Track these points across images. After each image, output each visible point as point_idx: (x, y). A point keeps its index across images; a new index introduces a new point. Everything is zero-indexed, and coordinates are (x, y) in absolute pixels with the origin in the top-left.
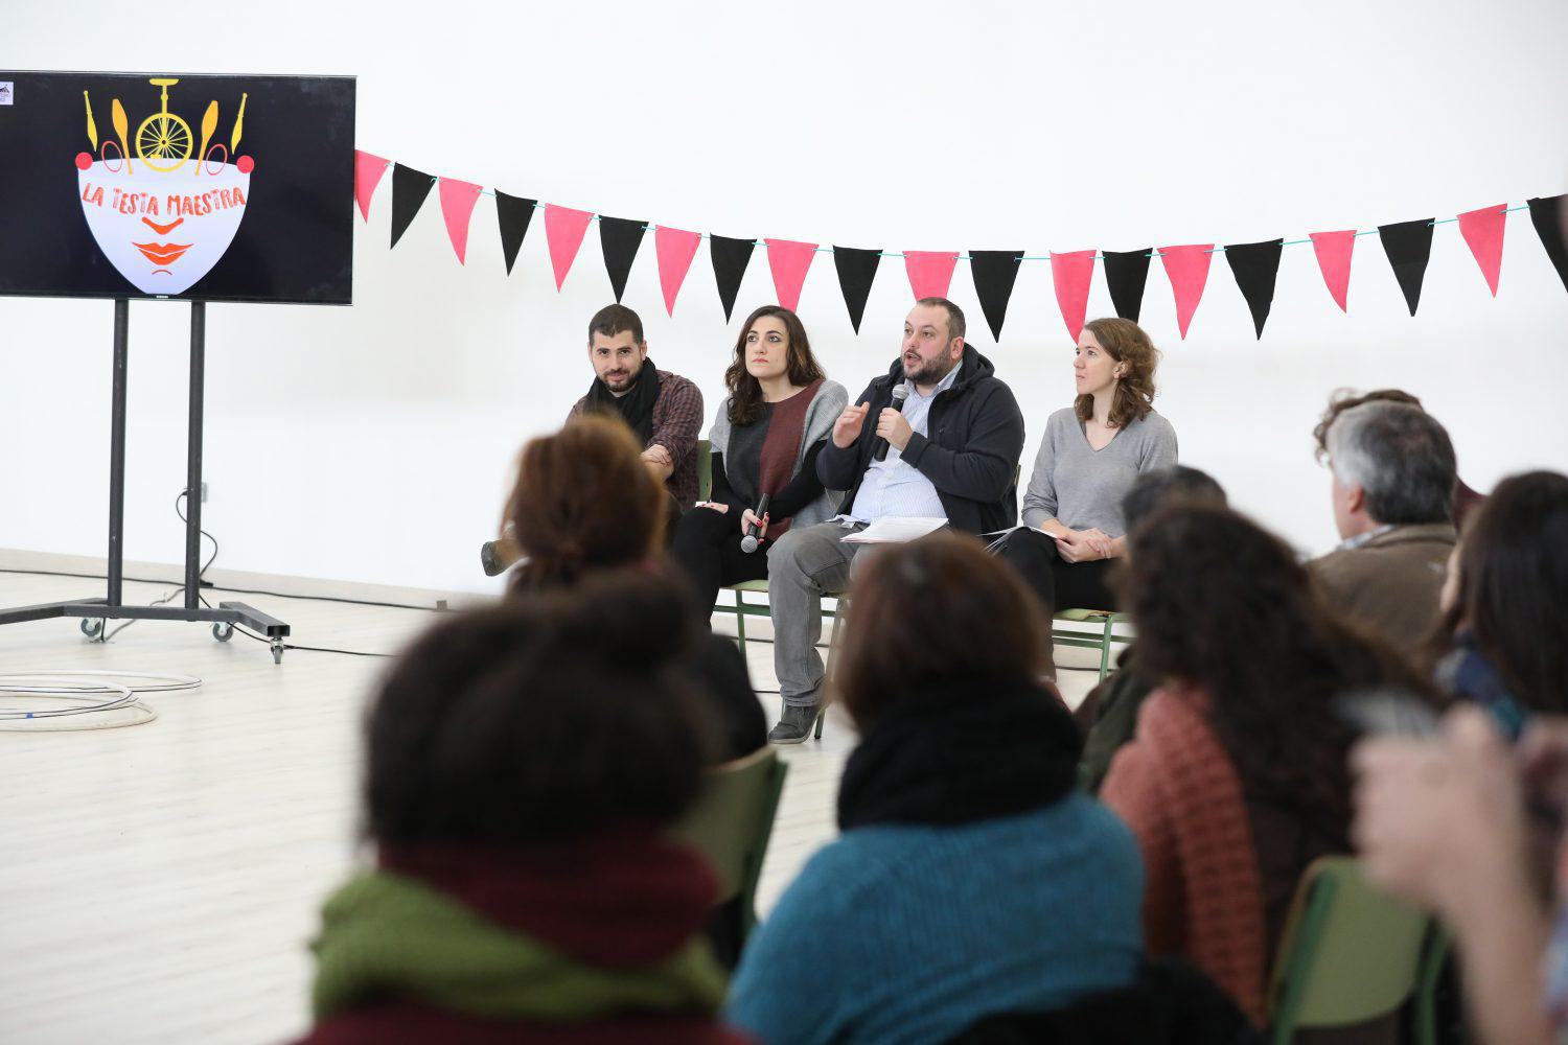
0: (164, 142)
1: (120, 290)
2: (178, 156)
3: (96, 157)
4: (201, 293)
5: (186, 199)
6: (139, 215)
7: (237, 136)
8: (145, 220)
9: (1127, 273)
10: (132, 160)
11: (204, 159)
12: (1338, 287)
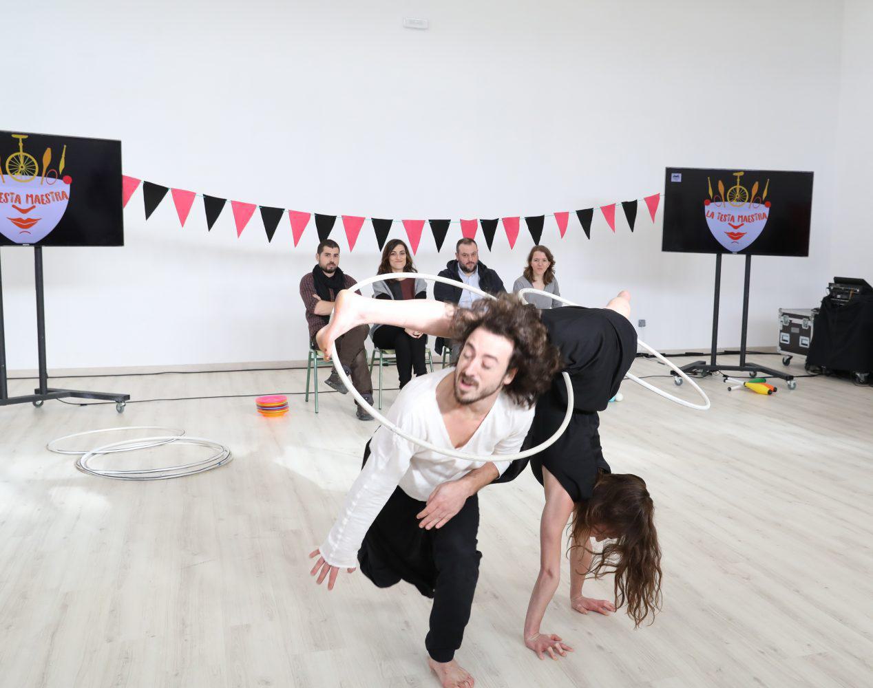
0: (22, 167)
1: (719, 249)
2: (30, 174)
3: (712, 201)
4: (749, 251)
5: (37, 196)
6: (10, 204)
7: (765, 195)
8: (14, 206)
9: (536, 225)
10: (4, 175)
11: (45, 176)
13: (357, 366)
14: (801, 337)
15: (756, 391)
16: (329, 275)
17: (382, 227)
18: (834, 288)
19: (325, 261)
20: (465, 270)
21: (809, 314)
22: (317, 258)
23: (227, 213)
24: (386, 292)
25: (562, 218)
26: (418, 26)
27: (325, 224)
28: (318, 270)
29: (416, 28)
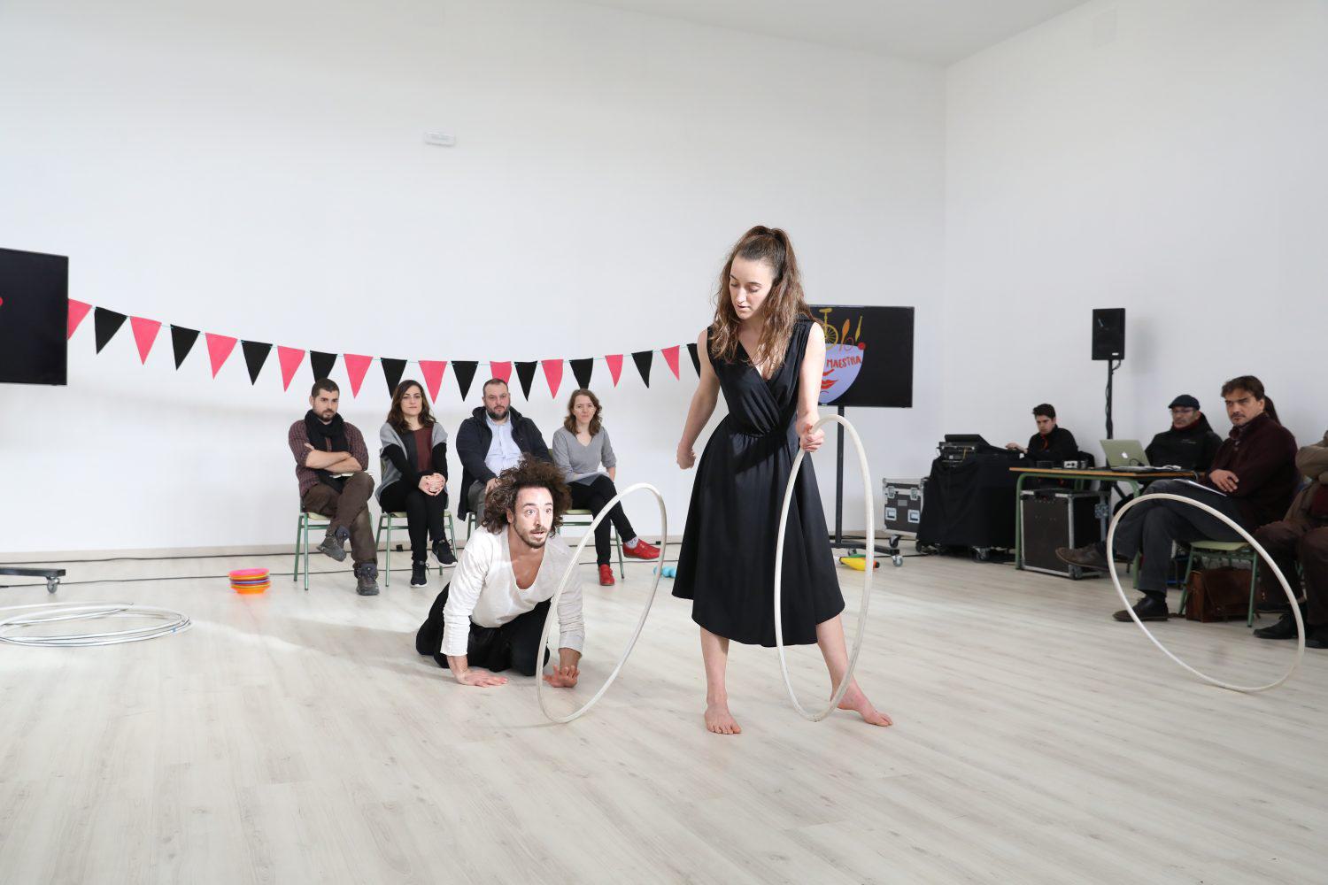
5: (835, 361)
9: (583, 369)
12: (616, 376)
13: (357, 529)
14: (910, 511)
15: (854, 566)
16: (326, 423)
17: (393, 368)
18: (946, 448)
19: (321, 407)
20: (495, 417)
21: (918, 483)
22: (311, 401)
23: (200, 349)
24: (395, 442)
25: (615, 363)
26: (444, 142)
27: (322, 363)
28: (312, 416)
29: (440, 145)
